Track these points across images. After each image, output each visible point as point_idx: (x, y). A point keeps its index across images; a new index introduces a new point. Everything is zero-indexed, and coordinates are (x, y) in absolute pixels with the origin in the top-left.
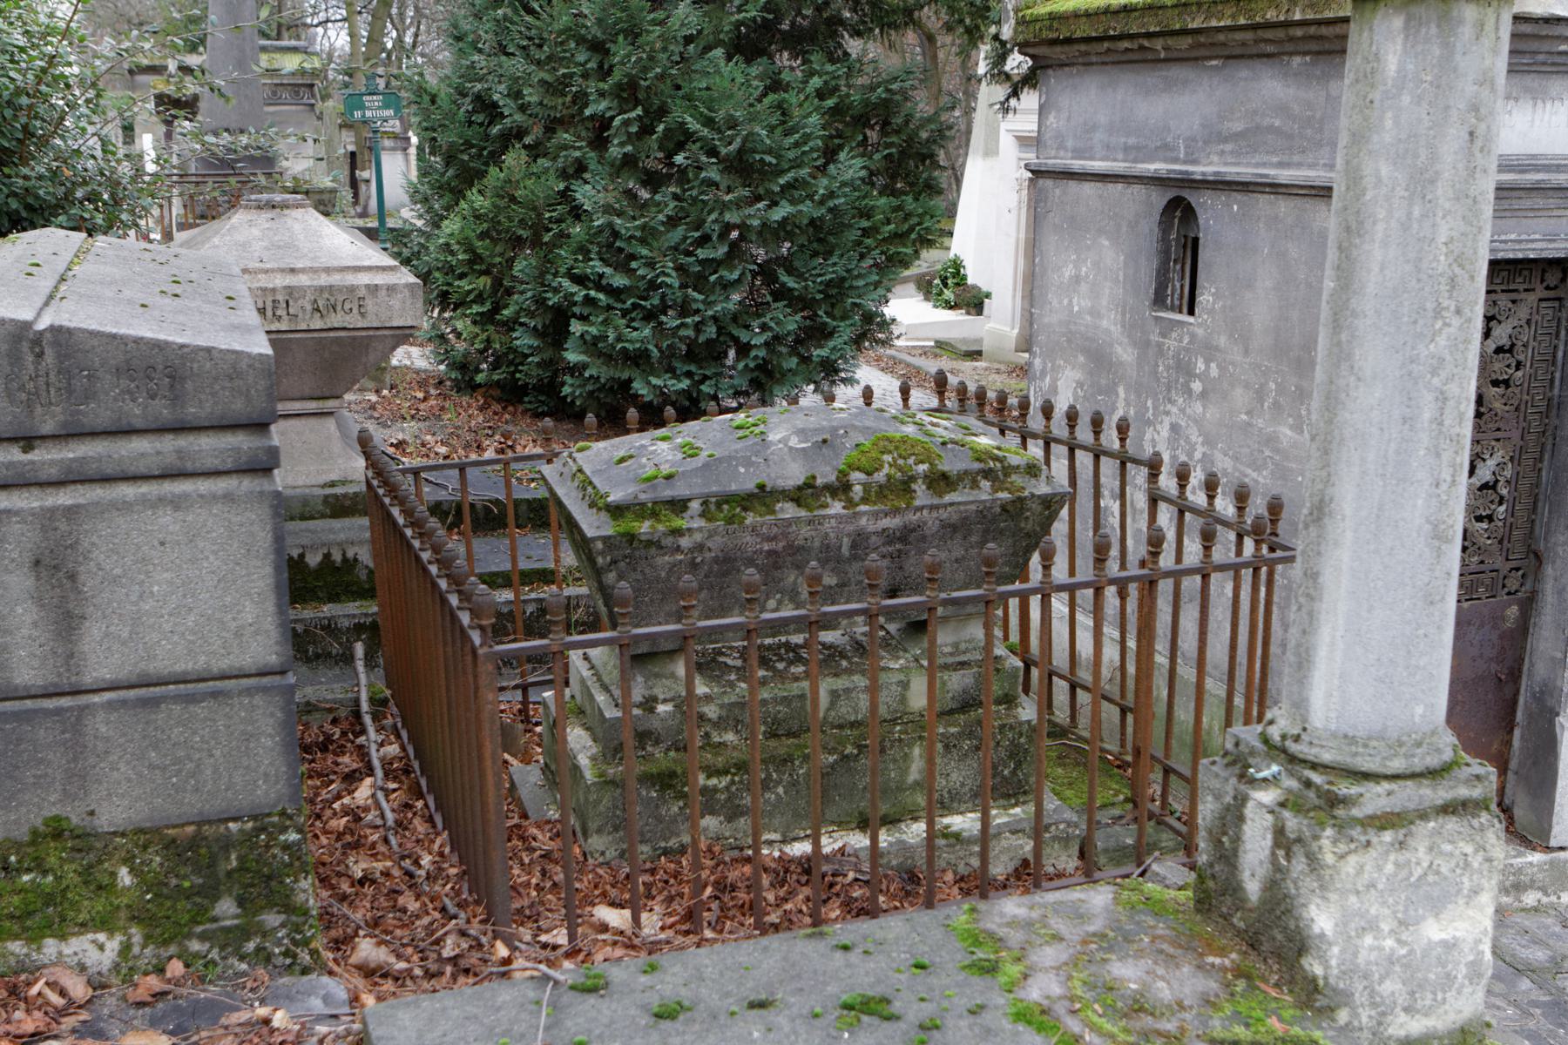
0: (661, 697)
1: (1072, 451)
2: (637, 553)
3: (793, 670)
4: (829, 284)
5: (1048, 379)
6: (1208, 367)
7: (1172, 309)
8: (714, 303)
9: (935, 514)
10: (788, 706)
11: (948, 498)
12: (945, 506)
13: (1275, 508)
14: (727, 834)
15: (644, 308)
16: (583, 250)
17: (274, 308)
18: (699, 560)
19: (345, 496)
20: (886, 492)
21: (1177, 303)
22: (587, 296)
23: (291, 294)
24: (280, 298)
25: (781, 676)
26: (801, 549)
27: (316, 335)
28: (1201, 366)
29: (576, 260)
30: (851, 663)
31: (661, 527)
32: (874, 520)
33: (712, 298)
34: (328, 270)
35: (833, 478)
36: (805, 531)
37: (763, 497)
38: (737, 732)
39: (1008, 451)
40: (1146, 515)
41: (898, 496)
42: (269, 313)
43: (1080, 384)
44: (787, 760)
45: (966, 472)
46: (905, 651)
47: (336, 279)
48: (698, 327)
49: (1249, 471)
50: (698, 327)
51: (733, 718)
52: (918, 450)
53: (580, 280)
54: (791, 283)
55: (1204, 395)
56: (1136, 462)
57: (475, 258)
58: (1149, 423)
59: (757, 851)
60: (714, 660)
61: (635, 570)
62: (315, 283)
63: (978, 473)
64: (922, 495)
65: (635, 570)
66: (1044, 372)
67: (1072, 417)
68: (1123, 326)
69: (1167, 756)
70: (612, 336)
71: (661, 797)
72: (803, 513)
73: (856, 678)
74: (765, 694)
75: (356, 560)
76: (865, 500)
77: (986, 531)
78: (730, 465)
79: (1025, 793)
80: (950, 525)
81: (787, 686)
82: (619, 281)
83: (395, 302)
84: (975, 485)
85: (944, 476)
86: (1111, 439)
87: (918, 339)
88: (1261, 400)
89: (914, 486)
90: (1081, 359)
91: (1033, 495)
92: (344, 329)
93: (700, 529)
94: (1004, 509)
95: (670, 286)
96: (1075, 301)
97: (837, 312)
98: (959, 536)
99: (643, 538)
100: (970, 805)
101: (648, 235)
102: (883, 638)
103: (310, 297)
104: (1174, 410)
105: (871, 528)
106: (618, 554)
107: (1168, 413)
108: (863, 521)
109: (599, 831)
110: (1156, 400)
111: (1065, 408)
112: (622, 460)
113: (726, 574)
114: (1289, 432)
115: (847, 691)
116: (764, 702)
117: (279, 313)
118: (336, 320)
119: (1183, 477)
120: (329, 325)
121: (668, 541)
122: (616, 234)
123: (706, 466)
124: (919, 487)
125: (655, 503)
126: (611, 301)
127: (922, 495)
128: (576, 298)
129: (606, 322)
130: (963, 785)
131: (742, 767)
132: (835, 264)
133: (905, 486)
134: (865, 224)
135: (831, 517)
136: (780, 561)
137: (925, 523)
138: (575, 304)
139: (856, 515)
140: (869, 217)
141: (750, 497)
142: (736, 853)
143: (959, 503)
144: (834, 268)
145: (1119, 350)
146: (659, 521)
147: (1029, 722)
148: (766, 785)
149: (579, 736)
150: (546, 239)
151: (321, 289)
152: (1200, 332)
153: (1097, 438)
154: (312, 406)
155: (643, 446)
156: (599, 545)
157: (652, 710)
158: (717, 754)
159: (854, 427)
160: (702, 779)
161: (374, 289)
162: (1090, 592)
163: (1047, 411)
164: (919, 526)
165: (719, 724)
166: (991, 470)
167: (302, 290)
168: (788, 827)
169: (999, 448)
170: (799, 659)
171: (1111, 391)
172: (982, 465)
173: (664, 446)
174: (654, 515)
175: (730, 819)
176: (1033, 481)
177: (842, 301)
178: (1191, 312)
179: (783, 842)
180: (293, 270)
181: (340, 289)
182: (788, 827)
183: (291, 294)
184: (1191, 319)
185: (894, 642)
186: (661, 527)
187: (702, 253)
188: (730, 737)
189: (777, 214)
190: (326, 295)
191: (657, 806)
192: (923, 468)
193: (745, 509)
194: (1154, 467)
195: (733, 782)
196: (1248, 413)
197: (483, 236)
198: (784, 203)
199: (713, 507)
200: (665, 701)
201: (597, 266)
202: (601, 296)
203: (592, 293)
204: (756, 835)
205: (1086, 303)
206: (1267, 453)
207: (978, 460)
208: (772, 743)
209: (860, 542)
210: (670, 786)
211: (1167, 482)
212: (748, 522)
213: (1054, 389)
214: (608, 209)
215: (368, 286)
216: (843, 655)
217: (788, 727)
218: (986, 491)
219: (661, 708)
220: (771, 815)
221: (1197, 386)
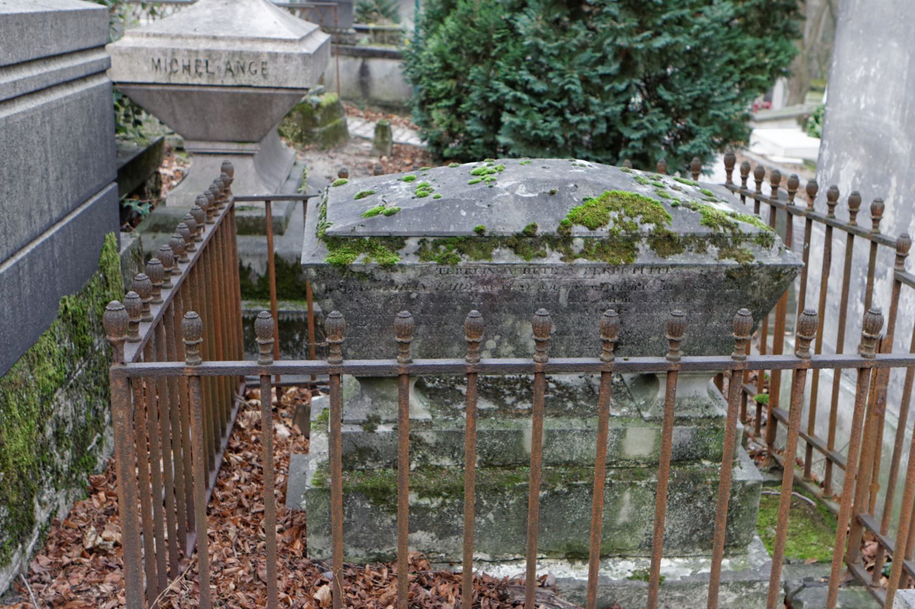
0: (384, 418)
2: (351, 284)
3: (520, 406)
4: (697, 99)
5: (832, 169)
8: (606, 107)
9: (655, 274)
10: (504, 440)
11: (670, 260)
12: (667, 267)
14: (438, 549)
15: (555, 107)
16: (517, 63)
17: (197, 66)
18: (414, 296)
19: (250, 218)
20: (607, 248)
22: (515, 97)
23: (210, 56)
24: (202, 58)
25: (505, 410)
26: (516, 295)
27: (229, 90)
29: (510, 70)
30: (576, 405)
31: (374, 261)
32: (590, 274)
33: (606, 103)
34: (242, 39)
35: (553, 229)
36: (520, 278)
37: (481, 241)
38: (454, 458)
39: (743, 219)
41: (619, 253)
42: (193, 70)
43: (859, 174)
44: (497, 490)
45: (693, 236)
46: (632, 399)
47: (247, 47)
48: (593, 124)
50: (593, 124)
51: (449, 444)
52: (647, 209)
53: (512, 84)
54: (666, 95)
57: (447, 67)
59: (468, 569)
60: (452, 388)
61: (351, 299)
62: (230, 48)
63: (707, 237)
64: (644, 253)
65: (351, 299)
66: (830, 163)
67: (854, 203)
68: (902, 121)
69: (883, 532)
70: (529, 125)
71: (375, 509)
72: (519, 260)
73: (574, 421)
74: (482, 427)
75: (249, 268)
76: (584, 254)
77: (711, 296)
78: (452, 207)
79: (735, 546)
80: (672, 287)
81: (506, 421)
82: (540, 87)
83: (291, 68)
84: (701, 249)
85: (669, 237)
87: (792, 157)
89: (637, 245)
90: (862, 151)
91: (761, 265)
92: (250, 86)
93: (413, 267)
94: (729, 275)
95: (575, 92)
96: (862, 99)
97: (702, 120)
98: (681, 299)
99: (355, 269)
100: (679, 551)
101: (563, 53)
102: (617, 385)
103: (224, 59)
105: (589, 281)
106: (333, 283)
108: (581, 274)
109: (316, 532)
111: (827, 188)
112: (362, 195)
113: (442, 312)
115: (563, 432)
116: (481, 434)
117: (200, 70)
118: (243, 79)
120: (238, 83)
121: (381, 275)
122: (540, 52)
123: (429, 206)
124: (643, 246)
125: (372, 237)
126: (533, 101)
127: (644, 253)
128: (507, 97)
129: (527, 115)
130: (672, 532)
131: (455, 491)
132: (702, 84)
133: (628, 244)
134: (731, 55)
135: (546, 267)
136: (497, 305)
137: (646, 282)
138: (507, 101)
139: (572, 267)
140: (737, 51)
141: (468, 239)
142: (442, 568)
143: (682, 266)
144: (702, 85)
145: (896, 143)
146: (373, 255)
147: (743, 482)
148: (478, 509)
149: (321, 443)
150: (493, 54)
151: (233, 54)
153: (831, 212)
154: (234, 147)
155: (388, 185)
156: (313, 273)
157: (371, 430)
158: (430, 477)
159: (585, 182)
160: (413, 498)
161: (274, 56)
162: (790, 372)
163: (833, 197)
164: (639, 285)
165: (436, 449)
166: (720, 236)
167: (219, 53)
168: (497, 549)
169: (733, 215)
170: (529, 396)
171: (884, 180)
172: (711, 230)
173: (404, 185)
174: (371, 249)
175: (442, 536)
176: (764, 251)
177: (707, 112)
179: (493, 562)
180: (215, 38)
181: (248, 55)
182: (497, 549)
183: (210, 56)
185: (624, 390)
186: (374, 261)
187: (601, 69)
188: (446, 462)
189: (659, 43)
190: (237, 59)
191: (371, 517)
192: (649, 227)
193: (461, 251)
195: (443, 504)
197: (455, 51)
198: (666, 34)
199: (429, 247)
200: (387, 422)
201: (525, 75)
202: (525, 97)
203: (519, 94)
204: (468, 551)
205: (872, 101)
207: (709, 224)
208: (487, 472)
209: (577, 292)
210: (384, 501)
212: (460, 264)
213: (837, 177)
214: (537, 34)
215: (270, 54)
216: (572, 397)
217: (502, 459)
218: (711, 256)
219: (382, 429)
220: (481, 537)
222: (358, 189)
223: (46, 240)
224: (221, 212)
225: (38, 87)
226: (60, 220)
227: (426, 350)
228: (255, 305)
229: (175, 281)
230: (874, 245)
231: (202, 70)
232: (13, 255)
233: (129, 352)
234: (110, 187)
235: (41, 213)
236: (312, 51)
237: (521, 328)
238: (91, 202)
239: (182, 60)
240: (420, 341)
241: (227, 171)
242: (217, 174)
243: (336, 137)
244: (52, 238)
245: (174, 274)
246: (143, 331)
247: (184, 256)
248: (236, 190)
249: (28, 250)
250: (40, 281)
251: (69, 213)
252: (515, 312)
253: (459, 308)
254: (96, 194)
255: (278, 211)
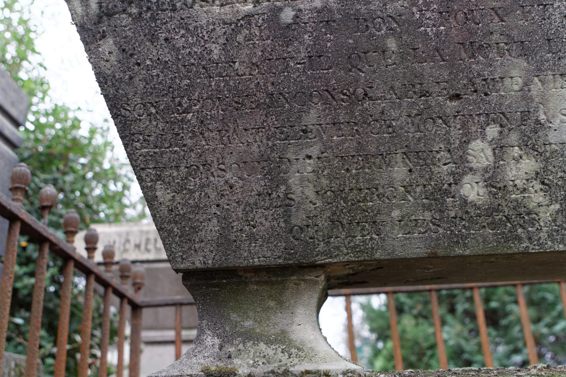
42: (143, 247)
61: (153, 38)
227: (330, 177)
228: (42, 228)
231: (151, 247)
237: (544, 101)
239: (134, 240)
240: (315, 151)
252: (525, 52)
253: (392, 44)
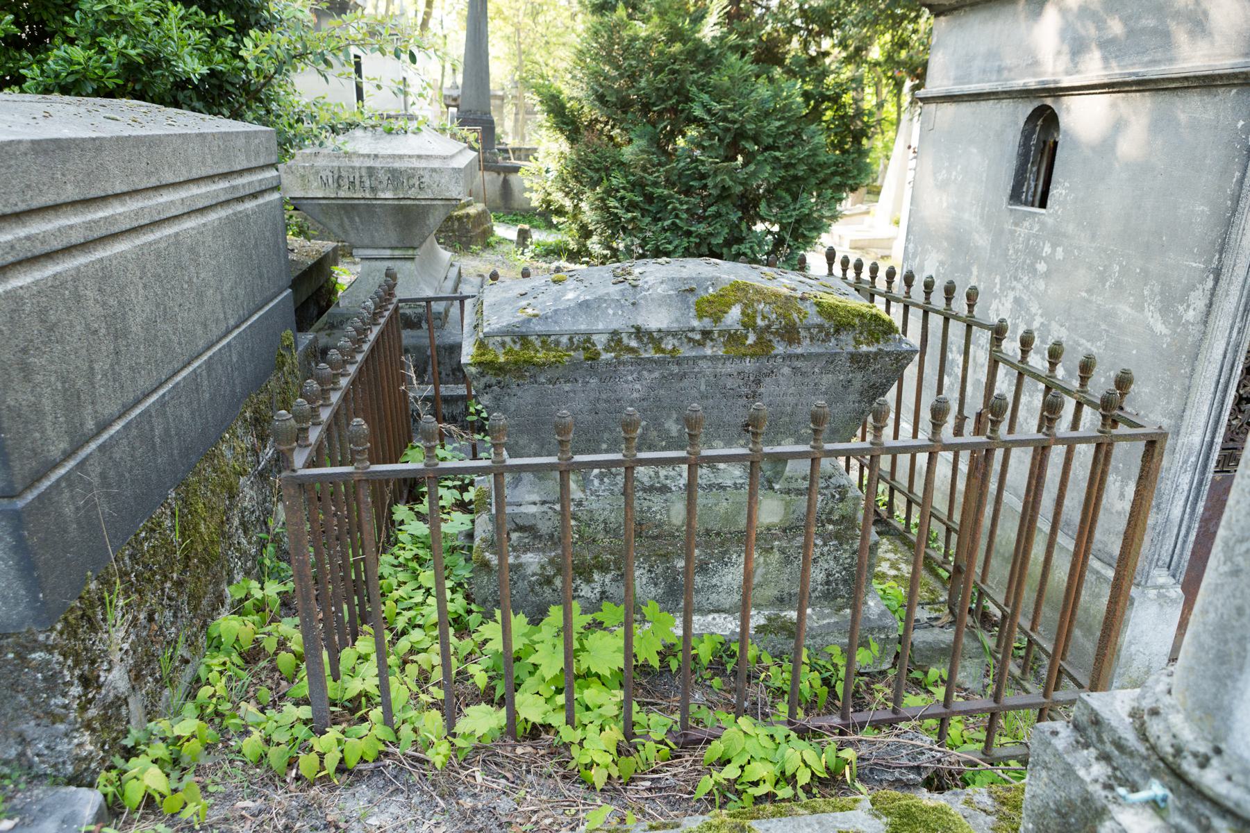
1: (926, 313)
6: (1054, 251)
7: (1026, 204)
13: (1123, 382)
21: (1030, 199)
28: (1047, 249)
40: (986, 369)
49: (1083, 341)
55: (1047, 275)
56: (982, 326)
58: (995, 296)
68: (982, 218)
86: (960, 305)
88: (1103, 280)
104: (1019, 286)
107: (1013, 289)
110: (1003, 277)
114: (1128, 310)
119: (1026, 343)
145: (976, 237)
152: (1050, 221)
178: (1043, 204)
184: (1042, 211)
194: (999, 332)
196: (1089, 291)
206: (1103, 327)
211: (1011, 347)
221: (1041, 267)
222: (509, 290)
223: (63, 477)
224: (387, 314)
225: (207, 204)
226: (237, 326)
229: (344, 382)
230: (947, 320)
232: (189, 363)
233: (299, 458)
234: (285, 294)
235: (217, 321)
236: (462, 166)
238: (267, 308)
241: (390, 274)
242: (380, 278)
243: (485, 240)
244: (229, 344)
245: (343, 375)
246: (314, 435)
247: (353, 357)
248: (400, 293)
249: (205, 358)
250: (219, 385)
251: (246, 320)
254: (272, 300)
255: (437, 307)
